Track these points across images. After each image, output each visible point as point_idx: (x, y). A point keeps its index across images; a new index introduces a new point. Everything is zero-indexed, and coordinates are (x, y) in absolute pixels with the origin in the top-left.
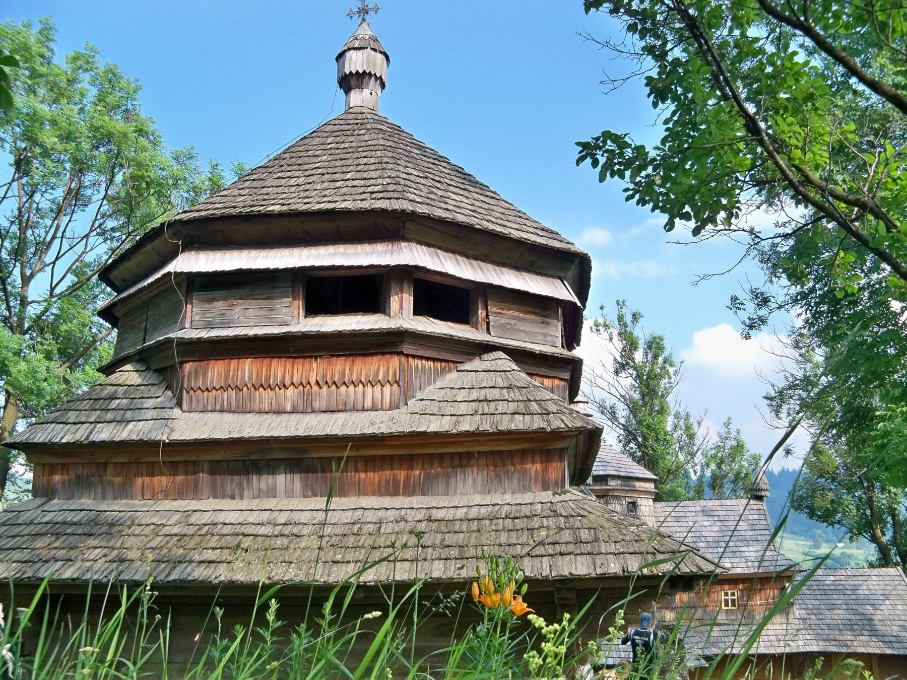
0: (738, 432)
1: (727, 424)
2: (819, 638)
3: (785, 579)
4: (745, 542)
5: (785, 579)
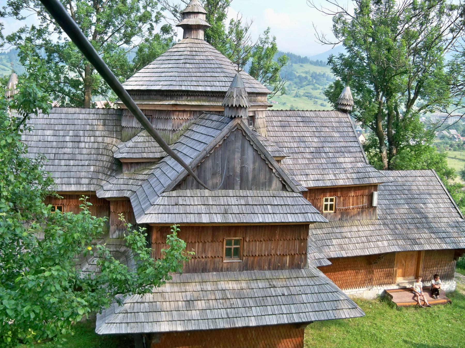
0: (274, 39)
1: (267, 32)
2: (397, 236)
3: (373, 188)
4: (341, 154)
5: (373, 188)
